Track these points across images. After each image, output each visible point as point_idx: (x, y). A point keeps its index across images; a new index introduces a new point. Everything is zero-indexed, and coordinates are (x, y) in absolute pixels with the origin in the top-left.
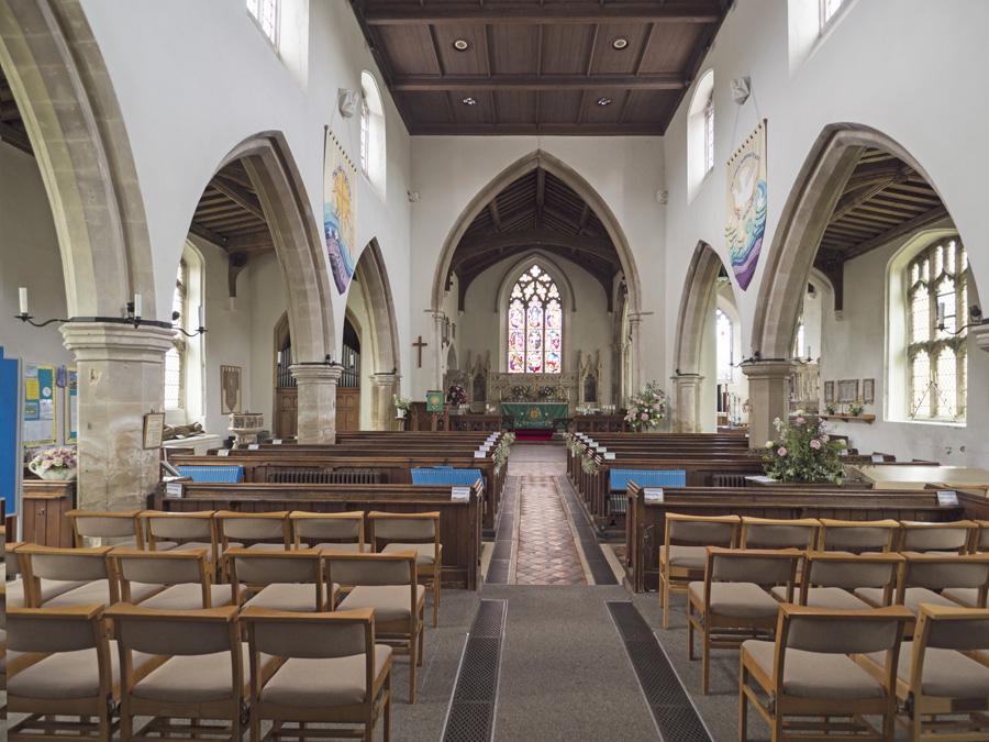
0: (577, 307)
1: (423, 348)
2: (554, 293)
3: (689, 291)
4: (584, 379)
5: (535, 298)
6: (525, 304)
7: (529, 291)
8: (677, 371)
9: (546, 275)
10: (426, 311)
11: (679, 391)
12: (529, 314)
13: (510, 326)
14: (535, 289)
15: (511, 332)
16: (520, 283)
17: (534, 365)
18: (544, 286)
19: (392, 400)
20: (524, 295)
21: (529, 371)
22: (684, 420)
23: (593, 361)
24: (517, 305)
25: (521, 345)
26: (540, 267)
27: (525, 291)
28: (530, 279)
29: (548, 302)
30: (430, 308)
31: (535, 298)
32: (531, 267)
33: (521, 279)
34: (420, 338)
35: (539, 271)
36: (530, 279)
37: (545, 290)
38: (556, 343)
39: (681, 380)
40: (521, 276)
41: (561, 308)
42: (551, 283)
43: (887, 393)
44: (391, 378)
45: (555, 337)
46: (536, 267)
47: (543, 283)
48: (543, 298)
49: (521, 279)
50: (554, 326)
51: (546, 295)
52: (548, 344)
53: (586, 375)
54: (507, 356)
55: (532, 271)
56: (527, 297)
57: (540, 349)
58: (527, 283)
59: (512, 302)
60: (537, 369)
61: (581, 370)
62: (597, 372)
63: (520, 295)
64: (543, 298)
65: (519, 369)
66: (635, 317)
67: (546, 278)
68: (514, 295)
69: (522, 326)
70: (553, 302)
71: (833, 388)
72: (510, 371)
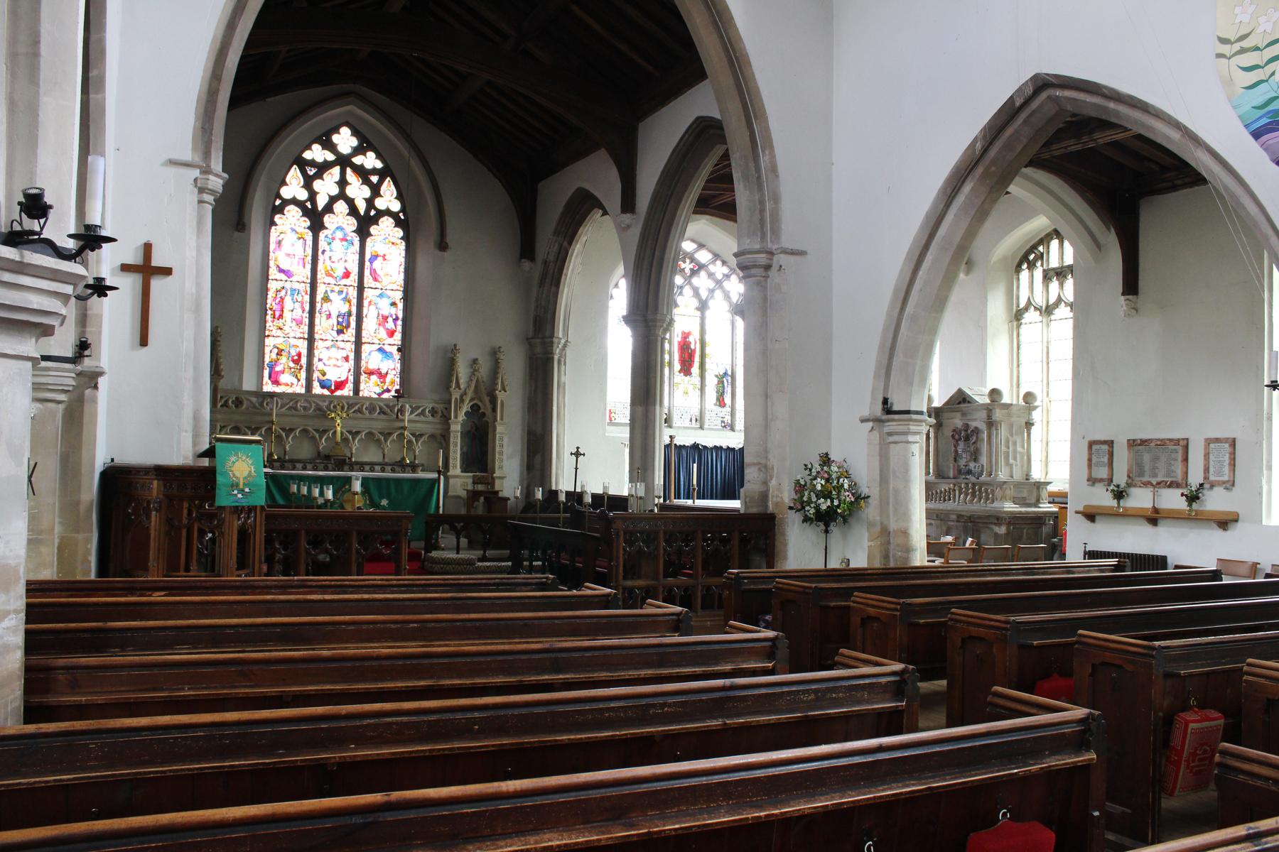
0: (449, 239)
1: (157, 284)
2: (389, 199)
3: (948, 205)
4: (462, 417)
5: (341, 207)
6: (316, 219)
7: (326, 187)
8: (885, 401)
9: (371, 155)
10: (173, 163)
11: (884, 456)
12: (322, 244)
13: (273, 272)
14: (343, 183)
15: (273, 286)
16: (303, 164)
17: (334, 375)
18: (366, 181)
19: (959, 466)
20: (313, 195)
21: (317, 390)
22: (893, 526)
23: (484, 370)
24: (292, 220)
25: (299, 323)
26: (356, 132)
27: (317, 185)
28: (330, 157)
29: (375, 221)
30: (187, 155)
31: (341, 207)
32: (336, 130)
33: (307, 155)
34: (148, 248)
35: (354, 142)
36: (330, 157)
37: (367, 192)
38: (390, 325)
39: (891, 427)
40: (309, 147)
41: (406, 238)
42: (383, 174)
43: (1270, 468)
44: (65, 376)
45: (386, 309)
46: (345, 131)
47: (362, 173)
48: (362, 207)
49: (307, 155)
50: (385, 281)
51: (370, 202)
52: (370, 324)
53: (466, 407)
54: (262, 346)
55: (335, 138)
56: (322, 202)
57: (350, 334)
58: (323, 168)
59: (280, 210)
60: (340, 385)
61: (456, 395)
62: (493, 400)
63: (303, 195)
64: (362, 207)
65: (291, 384)
66: (762, 259)
67: (370, 161)
68: (286, 193)
69: (304, 273)
70: (387, 222)
71: (1111, 455)
72: (268, 387)
